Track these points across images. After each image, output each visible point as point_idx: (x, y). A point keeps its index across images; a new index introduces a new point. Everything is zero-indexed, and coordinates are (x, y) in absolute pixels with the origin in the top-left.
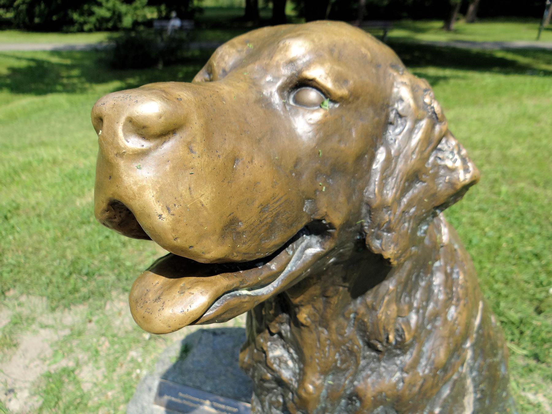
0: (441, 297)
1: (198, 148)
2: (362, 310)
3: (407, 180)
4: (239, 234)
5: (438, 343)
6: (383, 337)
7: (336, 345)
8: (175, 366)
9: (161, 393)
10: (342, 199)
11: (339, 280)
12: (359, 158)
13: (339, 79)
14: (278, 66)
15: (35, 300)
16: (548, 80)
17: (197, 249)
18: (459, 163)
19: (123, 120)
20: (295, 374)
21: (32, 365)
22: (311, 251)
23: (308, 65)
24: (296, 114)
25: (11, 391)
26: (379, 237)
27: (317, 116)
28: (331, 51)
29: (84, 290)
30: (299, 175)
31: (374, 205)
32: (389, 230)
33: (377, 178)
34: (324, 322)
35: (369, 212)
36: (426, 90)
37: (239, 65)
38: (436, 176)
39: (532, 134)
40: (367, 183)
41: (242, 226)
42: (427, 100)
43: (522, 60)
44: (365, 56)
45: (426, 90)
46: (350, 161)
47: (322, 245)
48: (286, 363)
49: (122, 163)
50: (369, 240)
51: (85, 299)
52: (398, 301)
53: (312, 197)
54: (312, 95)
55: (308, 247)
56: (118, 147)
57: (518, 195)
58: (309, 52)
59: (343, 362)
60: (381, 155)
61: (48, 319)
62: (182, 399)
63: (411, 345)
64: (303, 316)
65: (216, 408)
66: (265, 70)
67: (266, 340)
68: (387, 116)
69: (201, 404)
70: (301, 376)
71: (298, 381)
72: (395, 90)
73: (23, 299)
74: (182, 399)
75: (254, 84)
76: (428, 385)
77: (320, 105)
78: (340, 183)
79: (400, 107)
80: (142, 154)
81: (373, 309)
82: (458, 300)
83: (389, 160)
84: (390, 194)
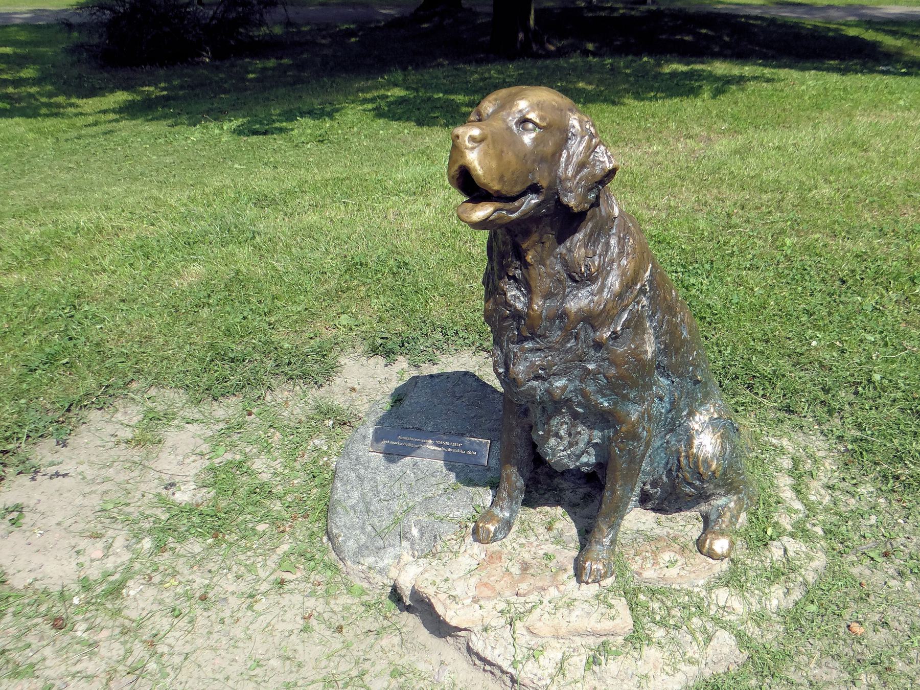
0: (616, 250)
1: (491, 147)
2: (564, 251)
3: (578, 167)
4: (505, 182)
5: (614, 279)
6: (579, 270)
7: (549, 275)
8: (389, 413)
9: (377, 438)
10: (546, 174)
11: (549, 229)
12: (554, 155)
13: (542, 118)
14: (514, 113)
15: (169, 393)
16: (913, 81)
17: (491, 185)
18: (606, 159)
19: (468, 136)
20: (525, 304)
21: (187, 461)
22: (533, 202)
23: (528, 113)
24: (524, 134)
25: (172, 485)
26: (566, 196)
27: (533, 135)
28: (538, 105)
29: (234, 379)
30: (526, 161)
31: (562, 178)
32: (571, 192)
33: (563, 165)
34: (542, 261)
35: (560, 182)
36: (587, 122)
37: (495, 112)
38: (594, 165)
39: (850, 169)
40: (558, 168)
41: (506, 179)
42: (588, 127)
43: (889, 41)
44: (554, 106)
45: (587, 122)
46: (549, 156)
47: (538, 198)
48: (519, 298)
49: (467, 151)
50: (561, 197)
51: (240, 387)
52: (586, 247)
53: (532, 172)
54: (530, 126)
55: (532, 199)
56: (466, 145)
57: (808, 249)
58: (528, 106)
59: (556, 288)
60: (565, 155)
61: (192, 412)
62: (402, 441)
63: (597, 278)
64: (529, 258)
65: (439, 446)
66: (509, 115)
67: (505, 283)
68: (567, 135)
69: (424, 443)
70: (529, 305)
71: (527, 307)
72: (570, 122)
73: (153, 392)
74: (402, 441)
75: (504, 121)
76: (610, 305)
77: (534, 130)
78: (545, 166)
79: (573, 130)
80: (473, 148)
81: (570, 251)
82: (628, 254)
83: (569, 156)
84: (570, 173)
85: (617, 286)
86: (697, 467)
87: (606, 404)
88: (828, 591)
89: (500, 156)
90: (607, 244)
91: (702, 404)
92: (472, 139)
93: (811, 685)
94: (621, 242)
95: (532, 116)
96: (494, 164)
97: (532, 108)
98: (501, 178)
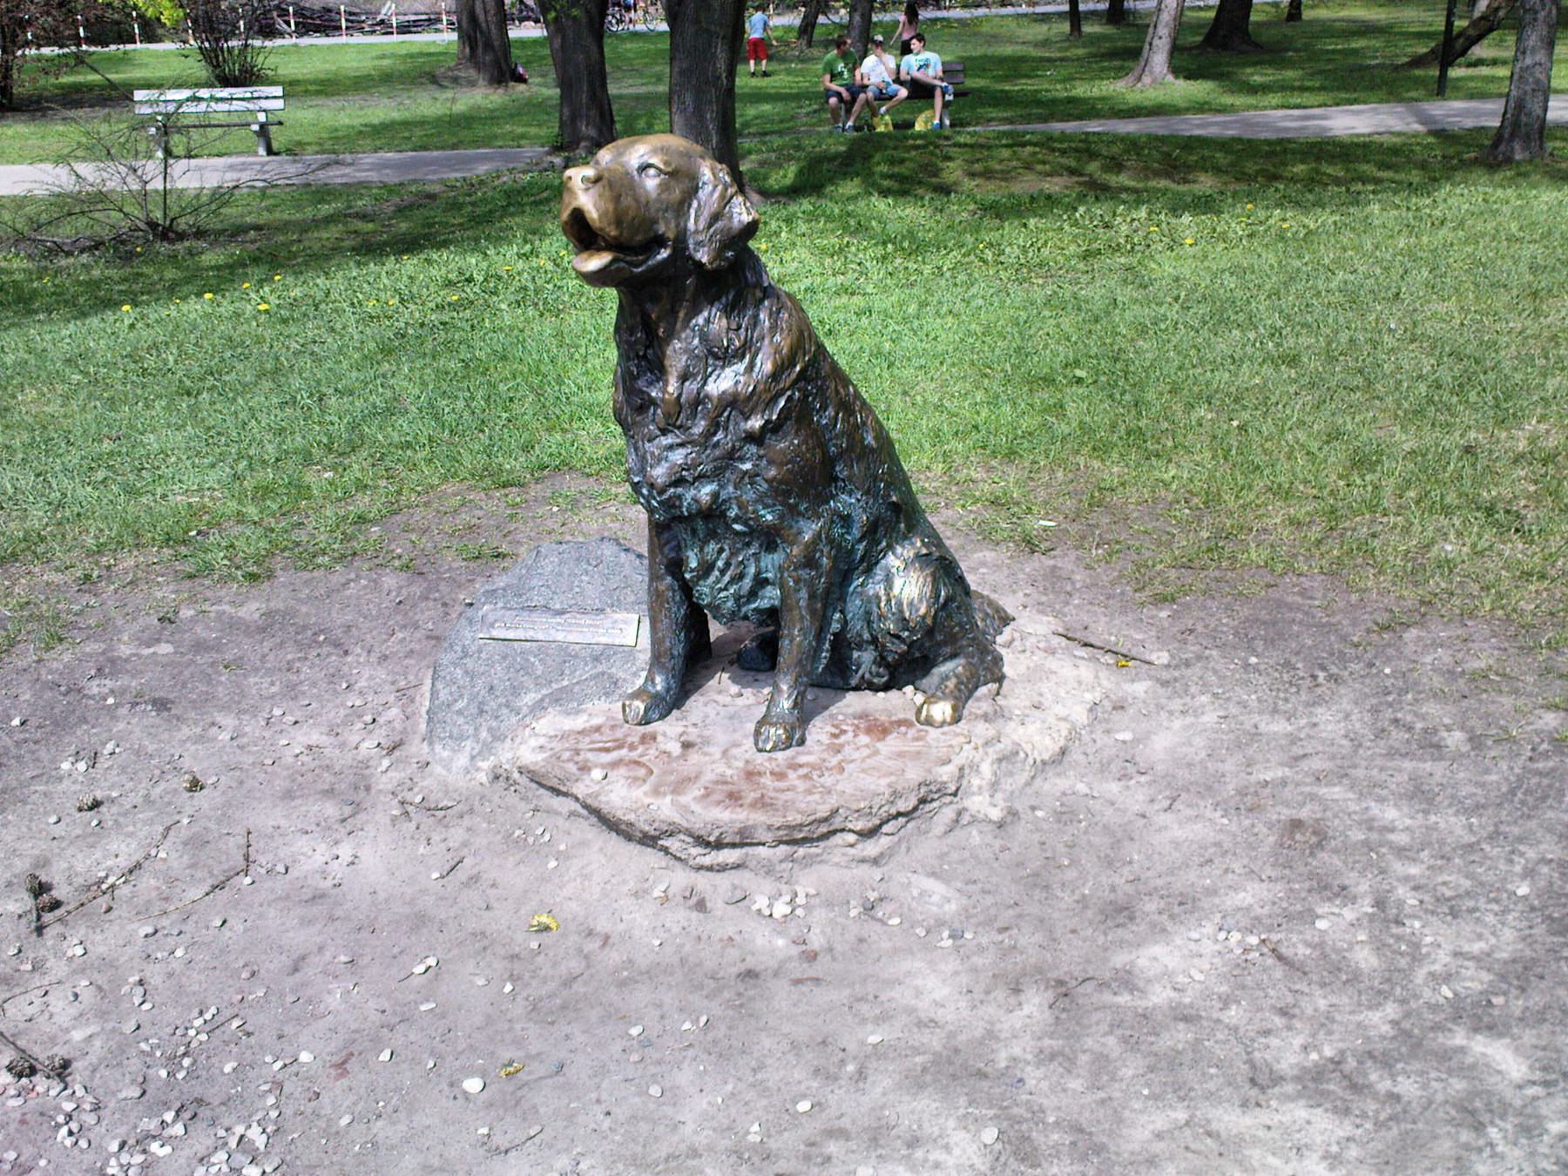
13: (666, 163)
60: (695, 204)
85: (768, 367)
86: (901, 612)
87: (769, 517)
88: (1437, 481)
89: (617, 199)
90: (756, 317)
91: (905, 538)
92: (585, 180)
93: (161, 705)
94: (775, 316)
95: (655, 161)
96: (611, 207)
97: (655, 151)
98: (618, 222)
